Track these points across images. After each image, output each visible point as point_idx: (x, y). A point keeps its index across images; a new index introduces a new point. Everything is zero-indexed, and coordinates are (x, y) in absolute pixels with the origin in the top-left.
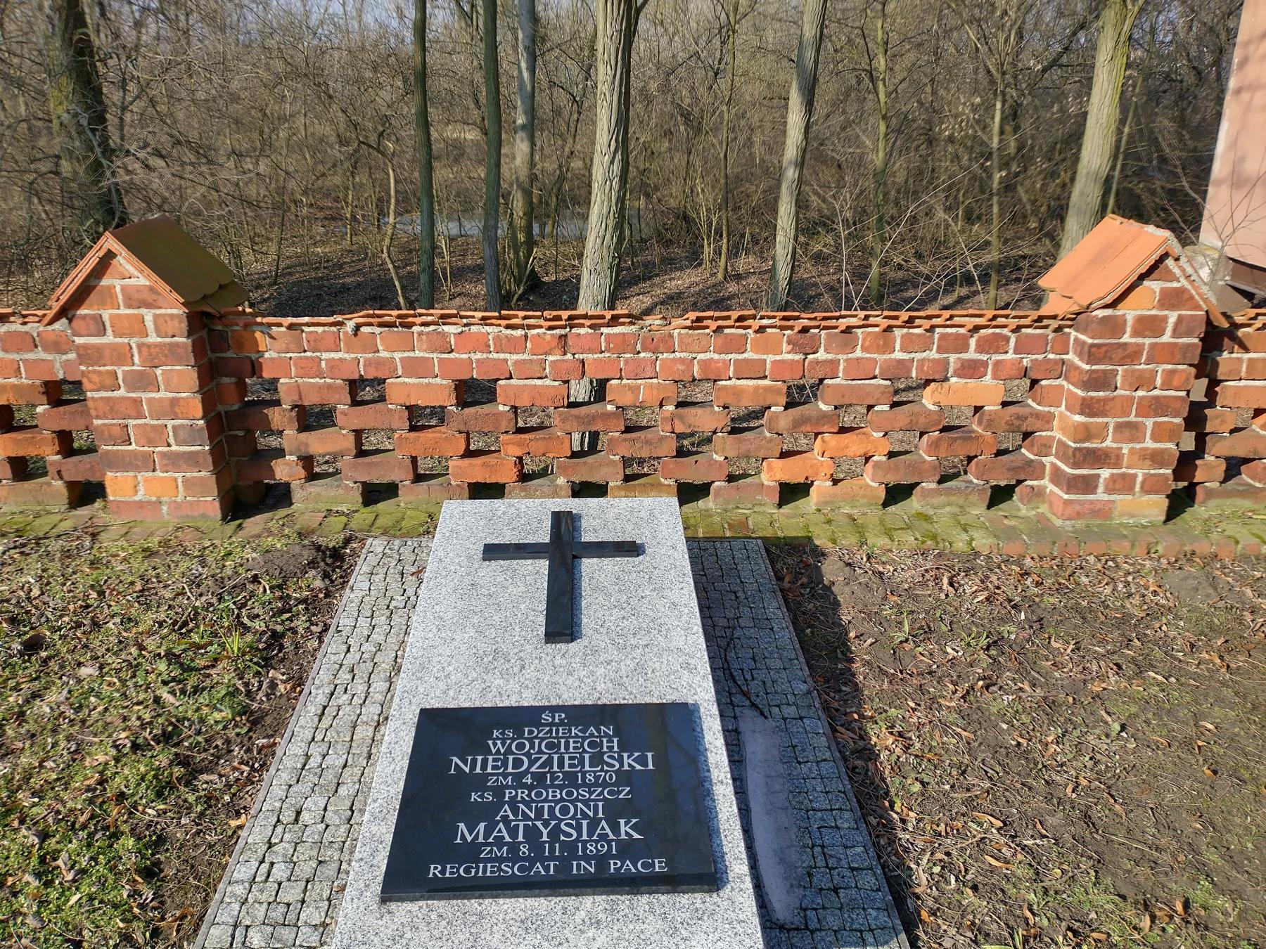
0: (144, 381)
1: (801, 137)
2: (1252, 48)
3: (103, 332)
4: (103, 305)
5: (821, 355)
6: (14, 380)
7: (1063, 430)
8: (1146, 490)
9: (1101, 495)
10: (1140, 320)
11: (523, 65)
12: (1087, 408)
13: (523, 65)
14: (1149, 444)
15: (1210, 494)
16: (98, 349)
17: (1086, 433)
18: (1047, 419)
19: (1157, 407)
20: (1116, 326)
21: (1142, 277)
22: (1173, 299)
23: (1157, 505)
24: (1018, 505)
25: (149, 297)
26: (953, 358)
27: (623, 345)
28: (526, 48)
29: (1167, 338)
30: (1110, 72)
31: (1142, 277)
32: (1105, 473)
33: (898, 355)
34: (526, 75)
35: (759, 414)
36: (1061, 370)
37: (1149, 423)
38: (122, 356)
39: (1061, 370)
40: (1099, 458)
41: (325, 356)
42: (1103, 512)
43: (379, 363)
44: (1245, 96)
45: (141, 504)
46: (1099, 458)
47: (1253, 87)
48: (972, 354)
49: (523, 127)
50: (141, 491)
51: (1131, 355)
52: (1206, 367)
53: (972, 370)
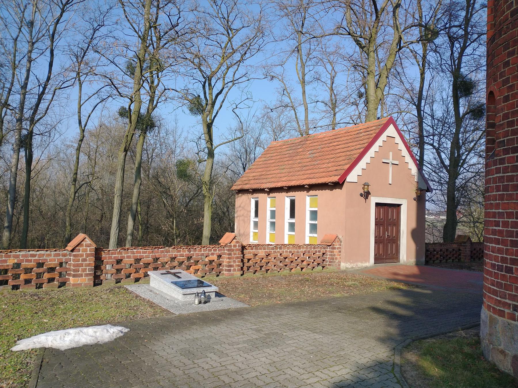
0: (84, 260)
1: (132, 228)
2: (238, 209)
3: (79, 251)
4: (81, 247)
5: (192, 252)
6: (54, 262)
7: (226, 263)
8: (238, 271)
9: (232, 272)
10: (234, 245)
11: (9, 206)
12: (229, 258)
13: (9, 206)
14: (237, 264)
15: (246, 272)
16: (78, 255)
17: (229, 262)
18: (223, 261)
19: (237, 258)
20: (231, 246)
21: (233, 239)
22: (237, 242)
23: (239, 273)
24: (220, 277)
25: (89, 245)
26: (210, 252)
27: (162, 252)
28: (11, 201)
29: (237, 248)
30: (208, 213)
31: (233, 239)
32: (232, 268)
33: (202, 252)
34: (10, 209)
35: (183, 262)
36: (225, 254)
37: (237, 260)
38: (82, 255)
39: (225, 254)
40: (231, 266)
41: (113, 256)
42: (232, 275)
43: (123, 257)
44: (238, 218)
45: (79, 284)
46: (231, 266)
47: (239, 216)
48: (212, 252)
49: (8, 227)
50: (79, 281)
51: (233, 250)
52: (243, 253)
53: (213, 254)
